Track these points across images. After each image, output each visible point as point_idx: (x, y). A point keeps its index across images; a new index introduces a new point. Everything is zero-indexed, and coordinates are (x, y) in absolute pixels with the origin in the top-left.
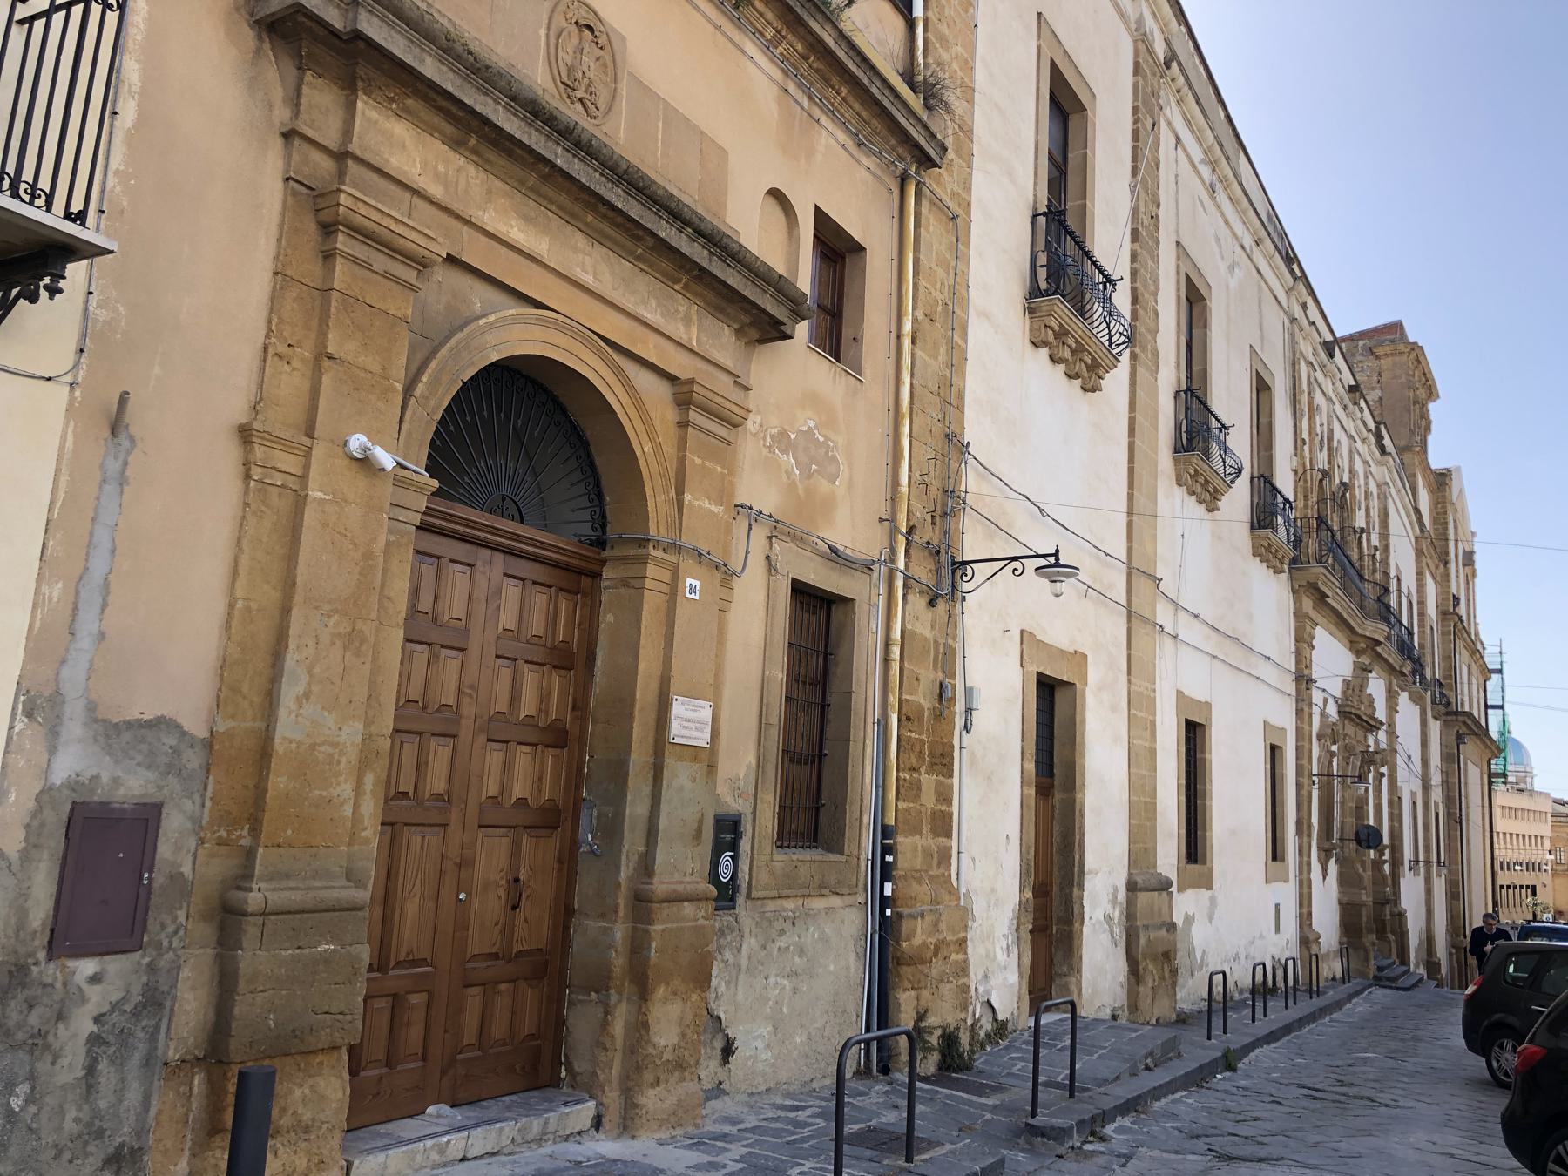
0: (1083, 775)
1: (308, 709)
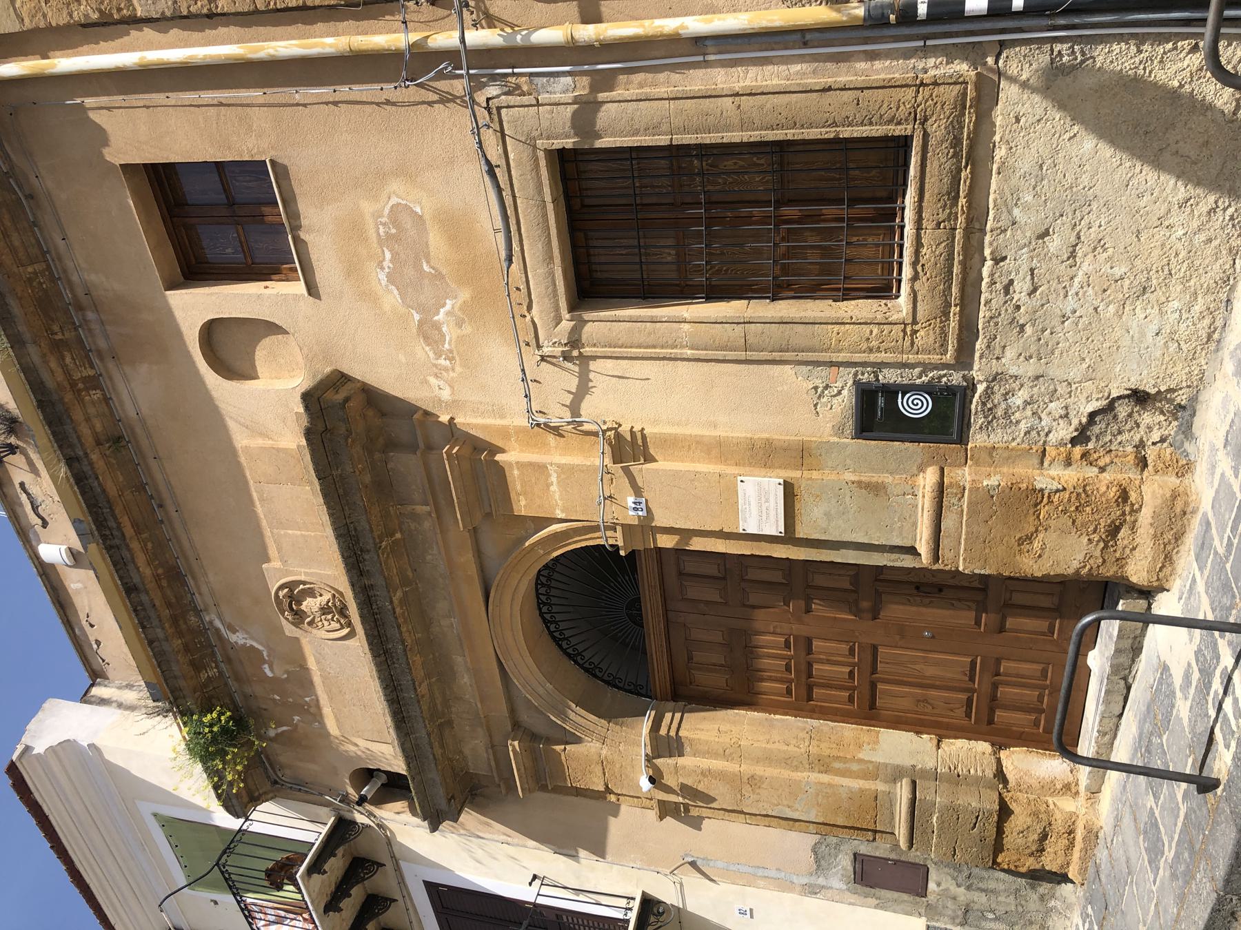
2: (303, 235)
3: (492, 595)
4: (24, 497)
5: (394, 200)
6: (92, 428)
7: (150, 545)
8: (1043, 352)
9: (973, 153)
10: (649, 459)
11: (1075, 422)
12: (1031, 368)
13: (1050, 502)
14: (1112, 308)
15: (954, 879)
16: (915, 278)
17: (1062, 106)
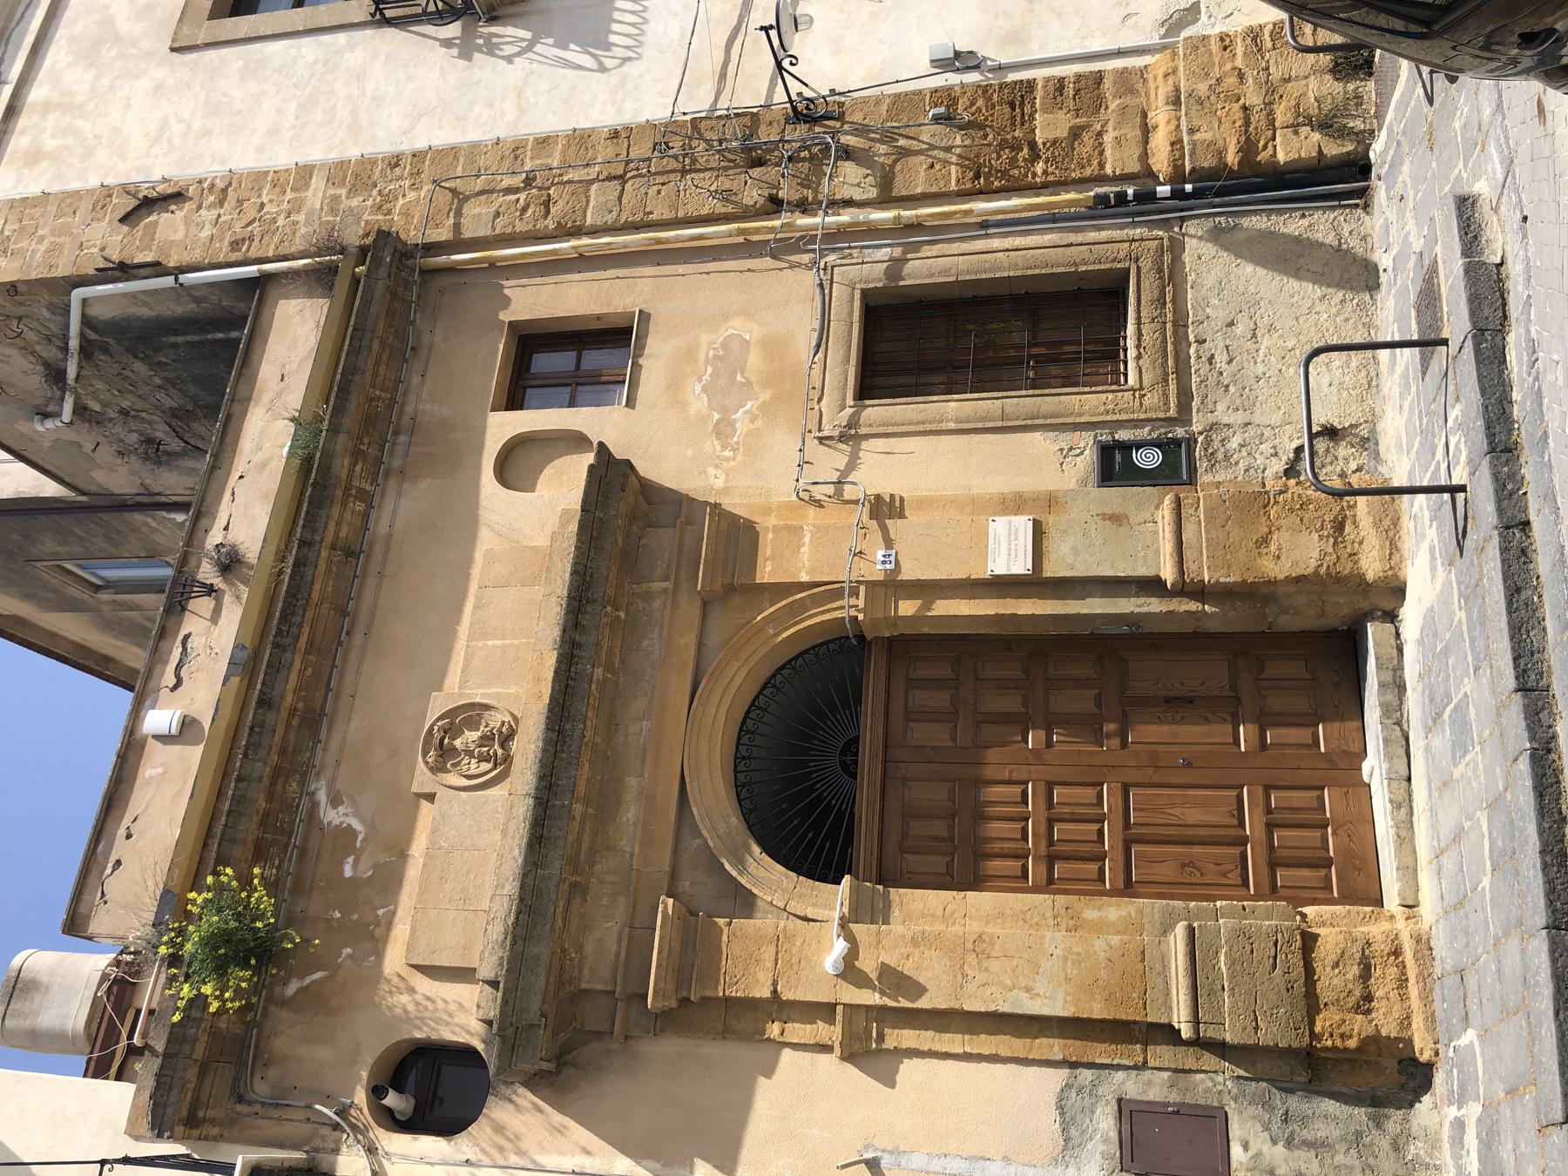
1: (1040, 987)
2: (641, 361)
3: (699, 692)
4: (177, 653)
5: (730, 331)
6: (337, 532)
7: (310, 671)
8: (1248, 406)
9: (1172, 276)
10: (901, 515)
11: (1284, 458)
12: (1240, 418)
13: (1276, 502)
14: (1292, 370)
16: (1139, 357)
17: (1227, 249)
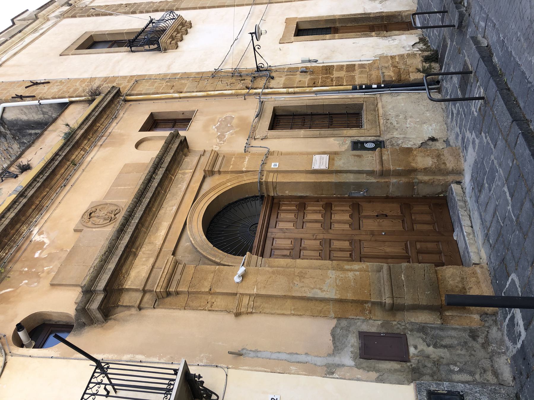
0: (329, 16)
1: (325, 288)
15: (424, 341)
